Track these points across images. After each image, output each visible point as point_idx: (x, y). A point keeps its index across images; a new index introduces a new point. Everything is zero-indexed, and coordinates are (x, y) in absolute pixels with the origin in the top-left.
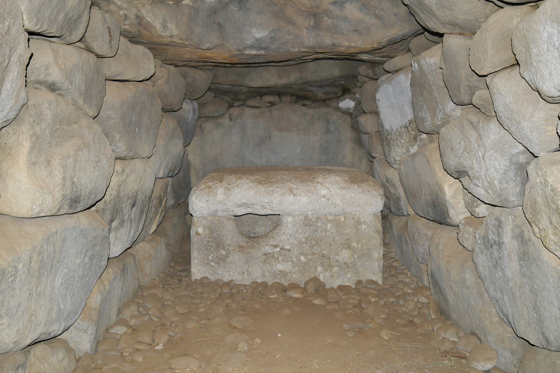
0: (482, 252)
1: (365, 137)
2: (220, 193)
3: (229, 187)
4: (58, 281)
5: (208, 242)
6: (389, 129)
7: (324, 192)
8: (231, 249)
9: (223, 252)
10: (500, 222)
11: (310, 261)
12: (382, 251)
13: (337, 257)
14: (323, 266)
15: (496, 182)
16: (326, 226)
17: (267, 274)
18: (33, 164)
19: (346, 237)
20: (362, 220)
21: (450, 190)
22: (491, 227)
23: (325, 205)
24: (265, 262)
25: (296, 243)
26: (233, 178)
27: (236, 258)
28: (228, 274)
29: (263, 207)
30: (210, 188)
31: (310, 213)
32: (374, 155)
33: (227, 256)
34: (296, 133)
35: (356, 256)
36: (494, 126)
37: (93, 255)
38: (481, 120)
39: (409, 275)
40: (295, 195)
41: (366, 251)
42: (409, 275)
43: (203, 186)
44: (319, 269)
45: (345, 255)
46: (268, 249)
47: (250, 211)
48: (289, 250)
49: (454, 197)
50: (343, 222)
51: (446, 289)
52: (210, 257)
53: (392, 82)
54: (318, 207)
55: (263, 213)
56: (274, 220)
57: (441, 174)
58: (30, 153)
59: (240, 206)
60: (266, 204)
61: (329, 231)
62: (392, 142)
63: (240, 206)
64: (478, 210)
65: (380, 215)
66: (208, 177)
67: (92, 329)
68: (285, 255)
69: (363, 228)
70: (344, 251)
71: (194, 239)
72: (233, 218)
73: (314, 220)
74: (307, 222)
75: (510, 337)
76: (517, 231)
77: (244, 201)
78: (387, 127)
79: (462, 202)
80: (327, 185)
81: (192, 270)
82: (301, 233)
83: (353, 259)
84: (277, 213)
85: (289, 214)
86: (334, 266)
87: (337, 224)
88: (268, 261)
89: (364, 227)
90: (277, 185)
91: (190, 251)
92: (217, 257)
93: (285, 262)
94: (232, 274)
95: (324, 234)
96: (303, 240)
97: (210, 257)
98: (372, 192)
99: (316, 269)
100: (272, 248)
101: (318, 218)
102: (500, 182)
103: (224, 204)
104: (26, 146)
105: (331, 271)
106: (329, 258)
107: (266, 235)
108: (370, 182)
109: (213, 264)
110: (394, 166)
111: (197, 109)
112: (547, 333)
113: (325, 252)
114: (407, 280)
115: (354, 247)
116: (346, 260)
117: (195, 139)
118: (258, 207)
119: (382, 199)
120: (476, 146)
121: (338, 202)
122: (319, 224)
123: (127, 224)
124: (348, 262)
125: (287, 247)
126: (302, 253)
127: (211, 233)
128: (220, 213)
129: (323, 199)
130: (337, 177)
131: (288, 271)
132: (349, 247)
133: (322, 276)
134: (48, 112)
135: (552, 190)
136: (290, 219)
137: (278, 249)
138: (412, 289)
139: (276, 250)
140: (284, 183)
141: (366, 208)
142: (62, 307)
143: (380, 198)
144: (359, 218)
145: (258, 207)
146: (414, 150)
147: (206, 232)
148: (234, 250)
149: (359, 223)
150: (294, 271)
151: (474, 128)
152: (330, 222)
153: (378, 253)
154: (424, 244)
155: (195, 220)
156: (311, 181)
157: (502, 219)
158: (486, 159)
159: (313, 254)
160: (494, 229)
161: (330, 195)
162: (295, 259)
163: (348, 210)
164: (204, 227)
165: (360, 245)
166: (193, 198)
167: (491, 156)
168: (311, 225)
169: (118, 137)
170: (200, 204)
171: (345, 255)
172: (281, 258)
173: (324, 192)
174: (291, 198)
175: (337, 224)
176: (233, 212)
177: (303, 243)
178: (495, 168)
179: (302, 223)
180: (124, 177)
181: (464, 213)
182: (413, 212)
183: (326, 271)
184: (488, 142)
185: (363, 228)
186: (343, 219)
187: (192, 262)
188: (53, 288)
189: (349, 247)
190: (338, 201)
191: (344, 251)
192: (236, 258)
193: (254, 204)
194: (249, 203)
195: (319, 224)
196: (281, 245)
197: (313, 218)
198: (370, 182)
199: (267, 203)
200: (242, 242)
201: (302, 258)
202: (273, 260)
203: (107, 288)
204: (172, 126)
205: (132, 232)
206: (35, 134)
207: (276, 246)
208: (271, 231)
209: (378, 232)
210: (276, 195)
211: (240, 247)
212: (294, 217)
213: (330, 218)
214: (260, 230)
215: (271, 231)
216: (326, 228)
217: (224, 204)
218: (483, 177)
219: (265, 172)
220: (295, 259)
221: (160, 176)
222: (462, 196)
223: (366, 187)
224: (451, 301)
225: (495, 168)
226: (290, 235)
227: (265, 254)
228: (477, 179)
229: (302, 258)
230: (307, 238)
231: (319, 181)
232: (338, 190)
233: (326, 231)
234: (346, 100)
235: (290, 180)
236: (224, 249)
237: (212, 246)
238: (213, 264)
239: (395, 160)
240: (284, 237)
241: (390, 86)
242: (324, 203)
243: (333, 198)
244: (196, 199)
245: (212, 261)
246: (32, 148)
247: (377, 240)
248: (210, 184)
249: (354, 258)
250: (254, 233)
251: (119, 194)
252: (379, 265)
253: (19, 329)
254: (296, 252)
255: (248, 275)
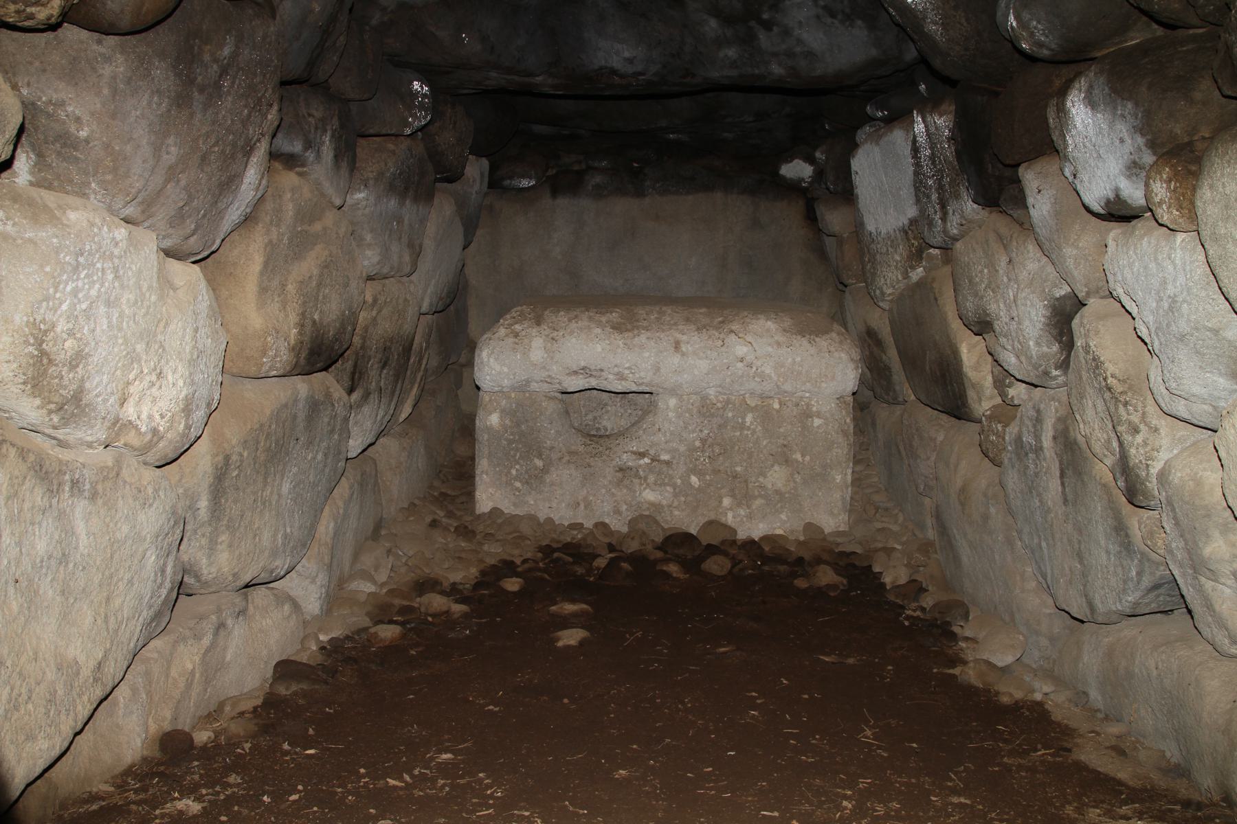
0: (1013, 467)
1: (829, 242)
2: (537, 348)
3: (555, 333)
4: (286, 487)
5: (510, 442)
6: (873, 231)
7: (741, 350)
8: (554, 456)
9: (539, 463)
10: (1038, 411)
11: (709, 485)
12: (850, 471)
13: (761, 479)
14: (733, 496)
15: (1031, 343)
16: (744, 418)
17: (625, 507)
18: (263, 290)
19: (781, 441)
20: (814, 409)
21: (970, 352)
22: (1027, 422)
23: (742, 376)
24: (619, 483)
25: (682, 448)
26: (562, 317)
27: (565, 478)
28: (547, 505)
29: (621, 377)
30: (516, 335)
31: (712, 392)
32: (846, 282)
33: (545, 470)
34: (691, 230)
35: (798, 478)
36: (1031, 248)
37: (329, 448)
38: (1015, 235)
39: (901, 519)
40: (683, 354)
41: (819, 470)
42: (901, 519)
43: (502, 331)
44: (726, 502)
45: (776, 477)
46: (627, 459)
47: (594, 383)
48: (668, 463)
49: (977, 367)
50: (778, 411)
51: (958, 537)
52: (514, 472)
53: (882, 142)
54: (728, 380)
55: (619, 388)
56: (640, 400)
57: (956, 325)
58: (262, 274)
59: (575, 373)
60: (627, 372)
61: (749, 429)
62: (878, 256)
63: (575, 373)
64: (1011, 392)
65: (850, 399)
66: (514, 314)
67: (322, 578)
68: (660, 473)
69: (815, 425)
70: (776, 468)
71: (482, 437)
72: (559, 396)
73: (719, 405)
74: (706, 409)
75: (1050, 614)
76: (1060, 427)
77: (583, 364)
78: (871, 226)
79: (990, 378)
80: (749, 338)
81: (477, 493)
82: (693, 432)
83: (792, 484)
84: (647, 389)
85: (673, 391)
86: (755, 498)
87: (766, 415)
88: (627, 482)
89: (817, 422)
90: (649, 334)
91: (473, 458)
92: (526, 472)
93: (660, 485)
94: (554, 505)
95: (738, 434)
96: (697, 444)
97: (514, 472)
98: (836, 354)
99: (721, 502)
100: (634, 457)
101: (728, 402)
102: (1038, 344)
103: (544, 368)
104: (256, 265)
105: (749, 507)
106: (746, 481)
107: (622, 434)
108: (834, 335)
109: (518, 484)
110: (881, 304)
111: (487, 174)
112: (1091, 594)
113: (738, 469)
114: (895, 528)
115: (797, 461)
116: (779, 485)
117: (479, 232)
118: (611, 377)
119: (857, 368)
120: (1005, 279)
121: (767, 372)
122: (730, 415)
123: (374, 397)
124: (783, 490)
125: (665, 457)
126: (694, 471)
127: (518, 425)
128: (534, 386)
129: (740, 365)
130: (769, 323)
131: (664, 502)
132: (786, 461)
133: (730, 515)
134: (290, 206)
135: (1094, 359)
136: (673, 402)
137: (647, 460)
138: (903, 544)
139: (642, 462)
140: (663, 331)
141: (824, 385)
142: (288, 530)
143: (851, 366)
144: (808, 405)
145: (611, 377)
146: (918, 273)
147: (507, 422)
148: (560, 459)
149: (807, 414)
150: (676, 504)
151: (1005, 247)
152: (753, 409)
153: (842, 476)
154: (928, 458)
155: (486, 398)
156: (717, 328)
157: (1042, 406)
158: (1019, 302)
159: (716, 472)
160: (1030, 424)
161: (752, 357)
162: (679, 481)
163: (787, 387)
164: (502, 411)
165: (807, 458)
166: (484, 354)
167: (1025, 298)
168: (712, 415)
169: (369, 237)
170: (498, 368)
171: (776, 477)
172: (651, 478)
173: (741, 350)
174: (676, 360)
175: (766, 415)
176: (560, 383)
177: (696, 449)
178: (1031, 320)
179: (695, 410)
180: (374, 313)
181: (991, 398)
182: (913, 397)
183: (739, 505)
184: (1023, 276)
185: (815, 425)
186: (776, 406)
187: (477, 479)
188: (280, 496)
189: (787, 461)
190: (768, 370)
191: (776, 468)
192: (565, 478)
193: (602, 370)
194: (593, 368)
195: (730, 415)
196: (652, 452)
197: (719, 401)
198: (834, 335)
199: (629, 368)
200: (578, 443)
201: (694, 480)
202: (636, 481)
203: (341, 511)
204: (448, 213)
205: (381, 413)
206: (270, 242)
207: (642, 455)
208: (633, 425)
209: (845, 433)
210: (647, 354)
211: (571, 453)
212: (680, 397)
213: (752, 402)
214: (609, 423)
215: (633, 425)
216: (744, 422)
217: (544, 368)
218: (1014, 334)
219: (625, 305)
220: (679, 481)
221: (424, 310)
222: (989, 366)
223: (824, 344)
224: (965, 559)
225: (1031, 320)
226: (672, 434)
227: (621, 470)
228: (1005, 336)
229: (694, 480)
230: (703, 441)
231: (733, 328)
232: (770, 349)
233: (742, 427)
234: (796, 161)
235: (675, 324)
236: (540, 456)
237: (517, 450)
238: (518, 484)
239: (883, 294)
240: (660, 438)
241: (876, 149)
242: (740, 372)
243: (759, 363)
244: (489, 356)
245: (517, 478)
246: (266, 264)
247: (841, 450)
248: (518, 327)
249: (795, 482)
250: (598, 429)
251: (364, 341)
252: (843, 499)
253: (240, 554)
254: (682, 469)
255: (586, 507)
